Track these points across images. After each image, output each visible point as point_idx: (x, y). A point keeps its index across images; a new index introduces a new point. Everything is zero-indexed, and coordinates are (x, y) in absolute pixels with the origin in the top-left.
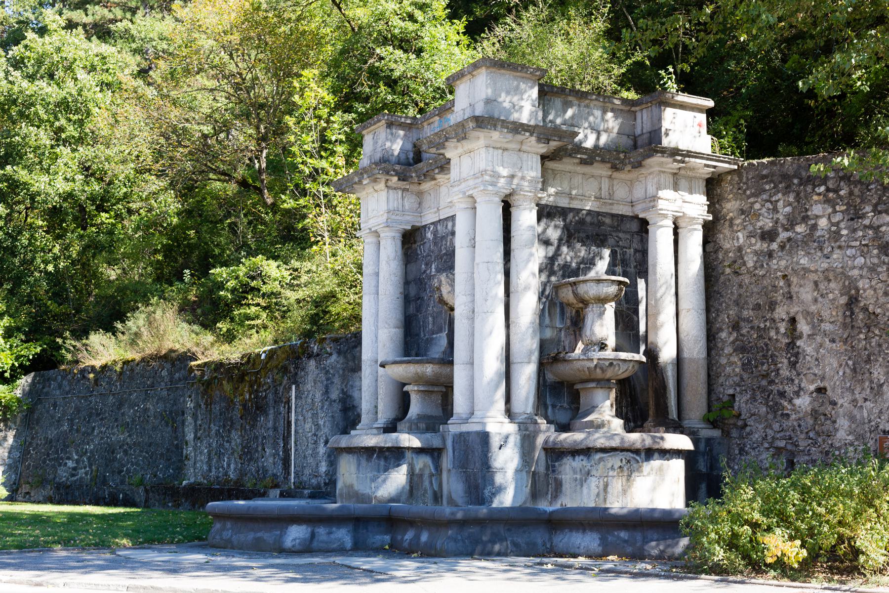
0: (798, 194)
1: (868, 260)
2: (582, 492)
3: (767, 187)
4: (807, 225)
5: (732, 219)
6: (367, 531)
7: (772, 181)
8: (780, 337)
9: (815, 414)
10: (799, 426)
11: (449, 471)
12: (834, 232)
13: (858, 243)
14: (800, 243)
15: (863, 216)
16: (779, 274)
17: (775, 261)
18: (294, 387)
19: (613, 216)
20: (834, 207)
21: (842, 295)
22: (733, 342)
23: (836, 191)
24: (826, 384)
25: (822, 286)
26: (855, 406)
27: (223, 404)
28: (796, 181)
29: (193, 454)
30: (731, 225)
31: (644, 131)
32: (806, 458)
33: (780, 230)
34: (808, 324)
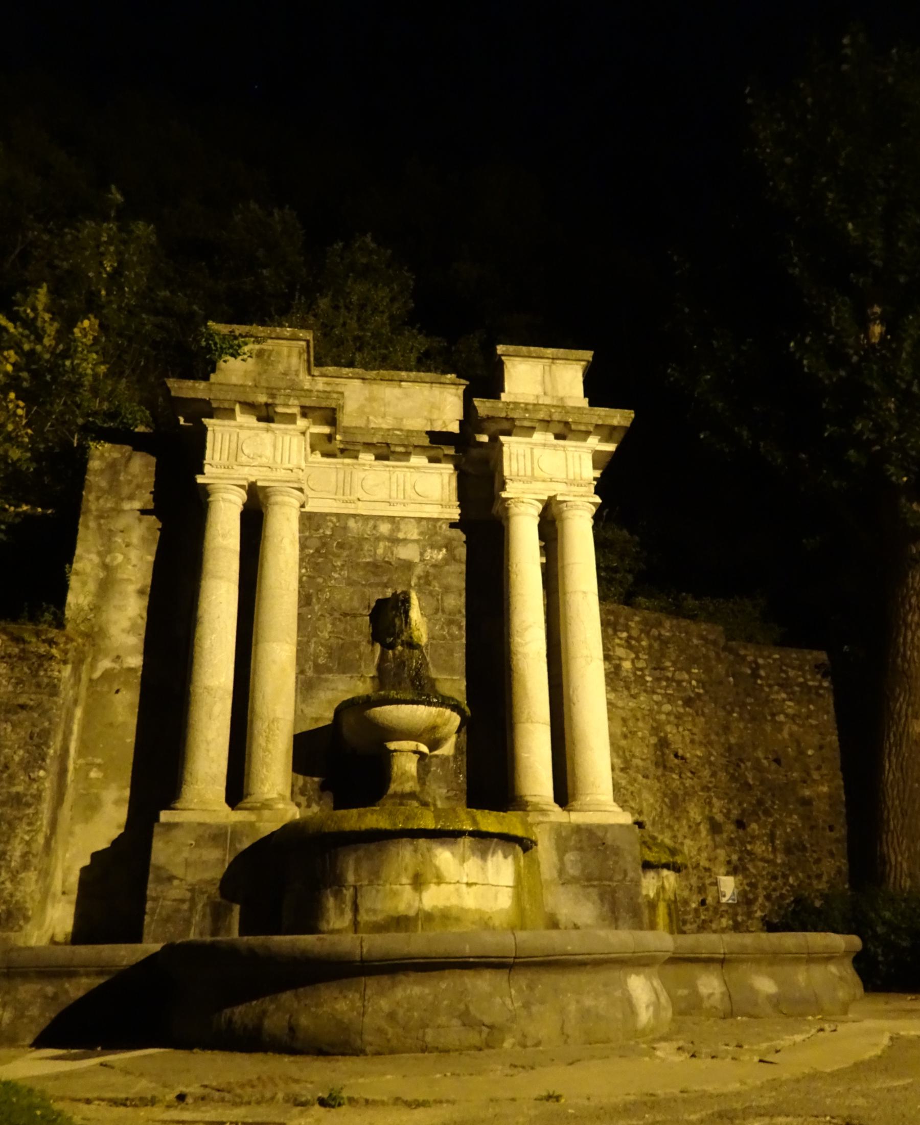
23: (638, 640)
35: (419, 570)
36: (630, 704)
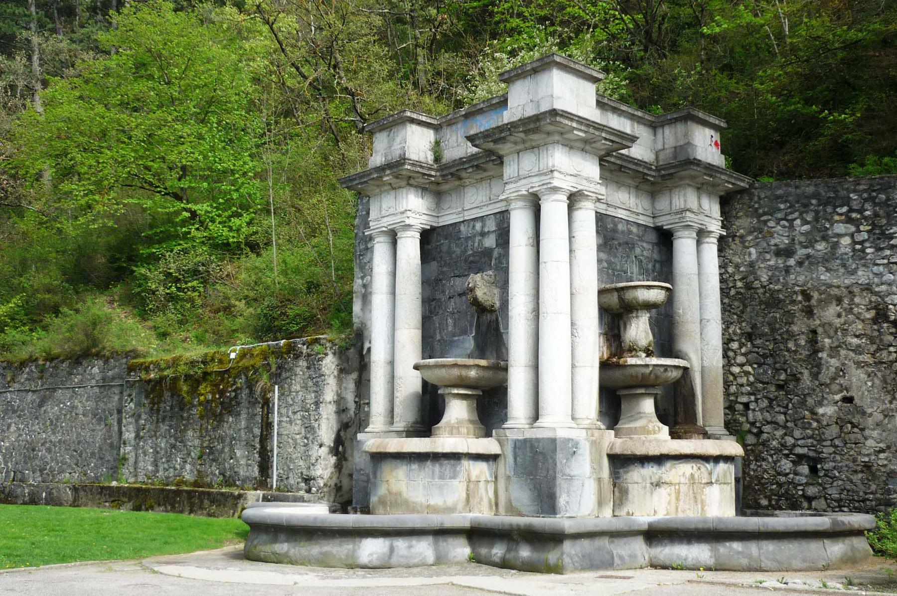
0: (817, 212)
3: (782, 206)
5: (742, 237)
6: (447, 544)
7: (786, 201)
9: (840, 422)
11: (508, 478)
12: (859, 250)
16: (797, 288)
17: (792, 277)
18: (277, 387)
19: (638, 225)
20: (858, 227)
21: (868, 310)
23: (861, 211)
28: (814, 202)
29: (133, 454)
31: (666, 146)
36: (846, 281)
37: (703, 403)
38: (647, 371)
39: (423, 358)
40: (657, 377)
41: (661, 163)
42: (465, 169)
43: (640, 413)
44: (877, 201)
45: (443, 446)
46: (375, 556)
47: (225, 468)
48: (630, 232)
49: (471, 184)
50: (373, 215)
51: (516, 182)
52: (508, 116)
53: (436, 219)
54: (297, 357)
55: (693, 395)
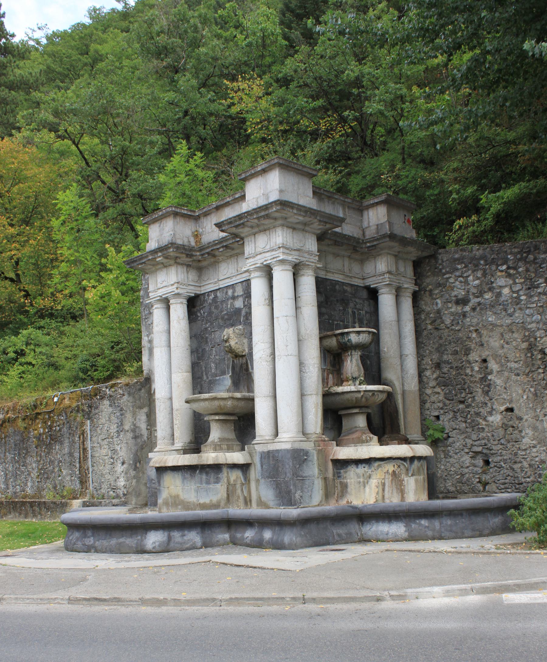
0: (484, 271)
1: (543, 317)
2: (364, 492)
4: (493, 293)
5: (431, 291)
7: (462, 263)
8: (474, 373)
9: (505, 427)
10: (493, 436)
11: (258, 481)
12: (516, 298)
13: (535, 305)
14: (488, 306)
15: (538, 287)
16: (472, 328)
17: (468, 320)
19: (352, 285)
21: (523, 342)
22: (436, 379)
24: (514, 405)
25: (507, 337)
26: (537, 420)
27: (17, 438)
28: (482, 262)
30: (431, 294)
31: (371, 224)
32: (499, 458)
33: (471, 297)
34: (497, 363)
35: (243, 313)
37: (405, 417)
38: (359, 395)
39: (194, 394)
40: (367, 399)
41: (367, 237)
42: (218, 249)
43: (356, 427)
44: (527, 260)
45: (207, 460)
46: (157, 544)
47: (55, 484)
48: (345, 291)
49: (223, 260)
50: (151, 288)
51: (254, 257)
52: (245, 207)
53: (199, 289)
54: (102, 398)
55: (397, 411)
